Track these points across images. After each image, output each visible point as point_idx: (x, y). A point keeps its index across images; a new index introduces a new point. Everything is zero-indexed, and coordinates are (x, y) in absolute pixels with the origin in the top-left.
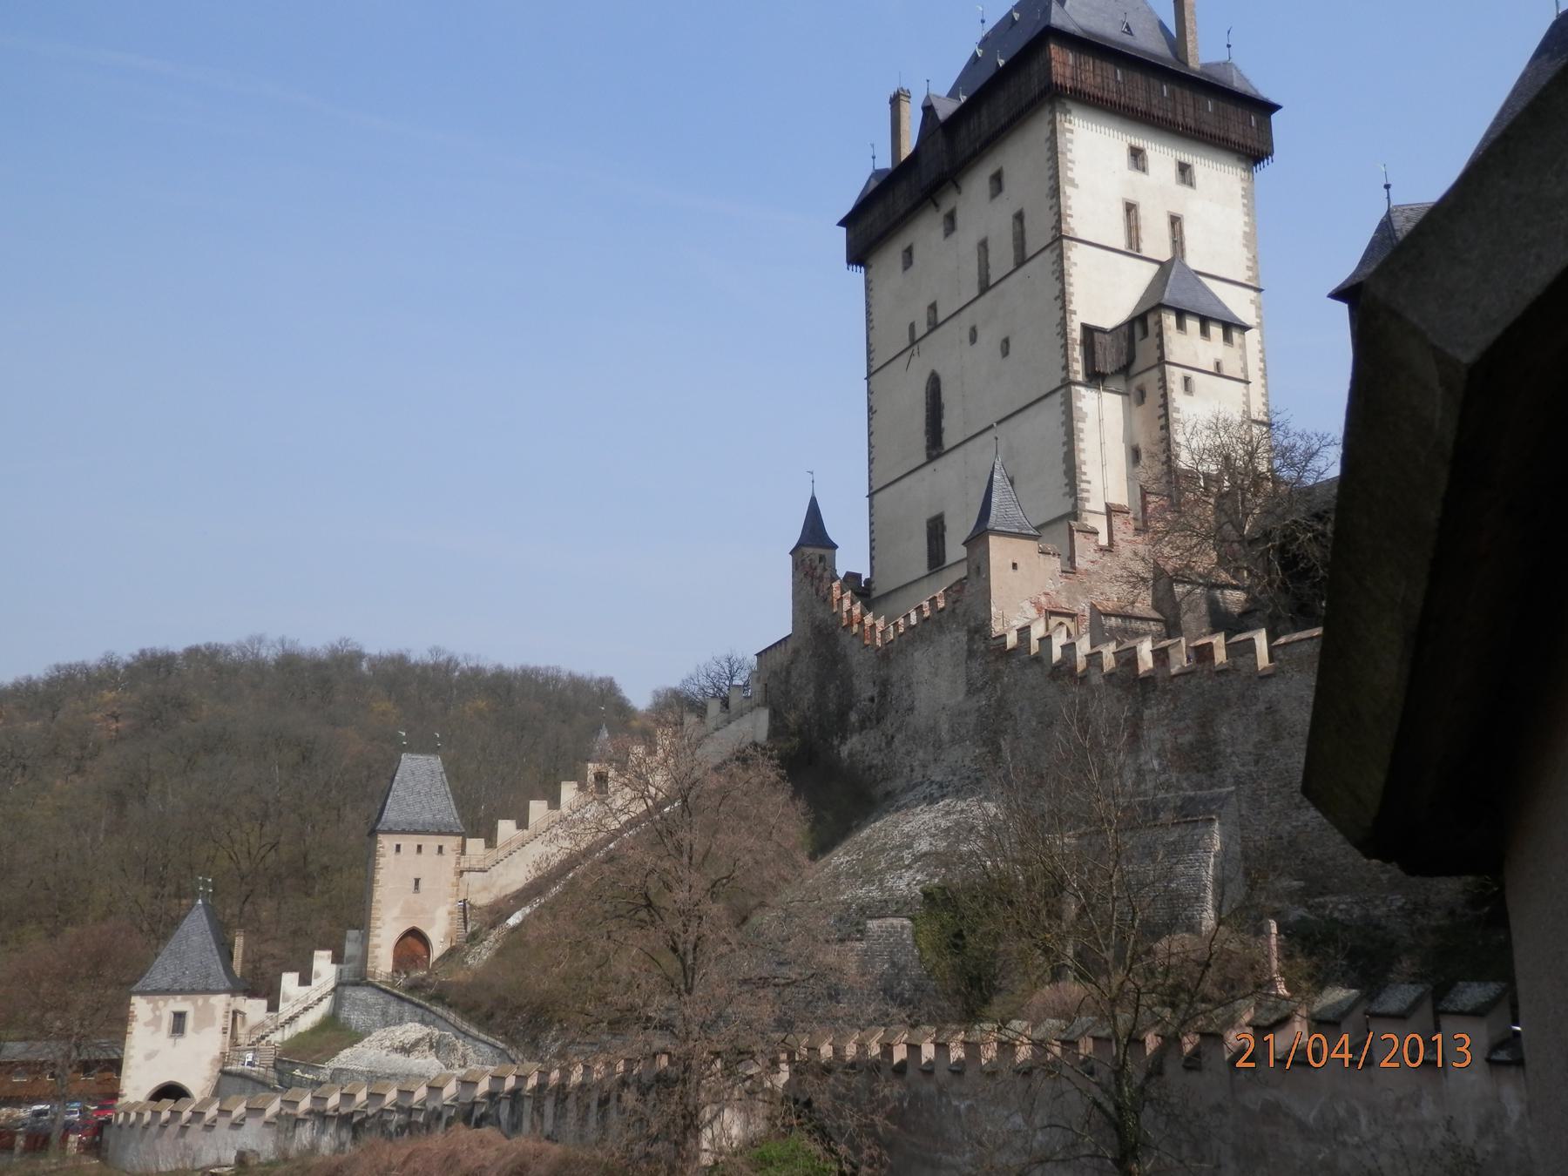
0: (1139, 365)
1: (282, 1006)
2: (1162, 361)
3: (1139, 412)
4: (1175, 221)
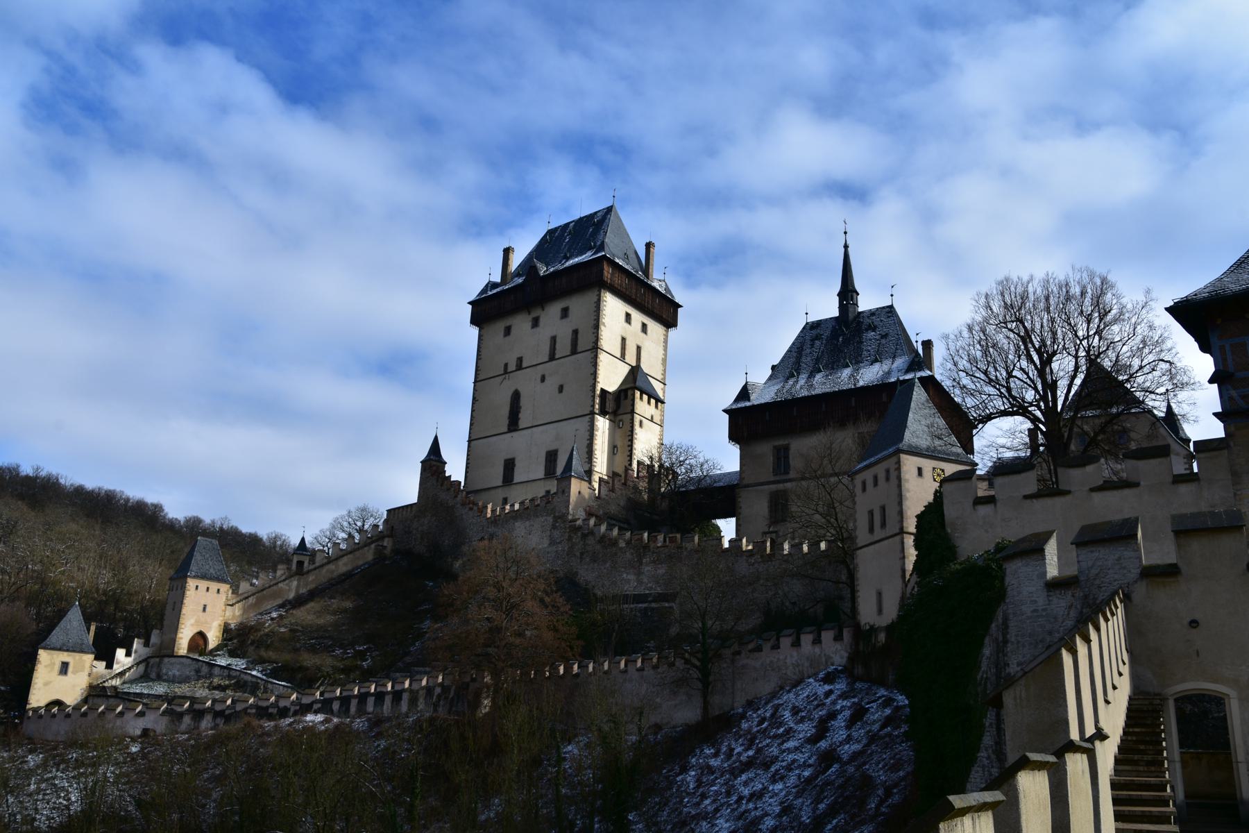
0: (620, 411)
1: (115, 666)
2: (632, 412)
3: (619, 433)
4: (639, 348)
